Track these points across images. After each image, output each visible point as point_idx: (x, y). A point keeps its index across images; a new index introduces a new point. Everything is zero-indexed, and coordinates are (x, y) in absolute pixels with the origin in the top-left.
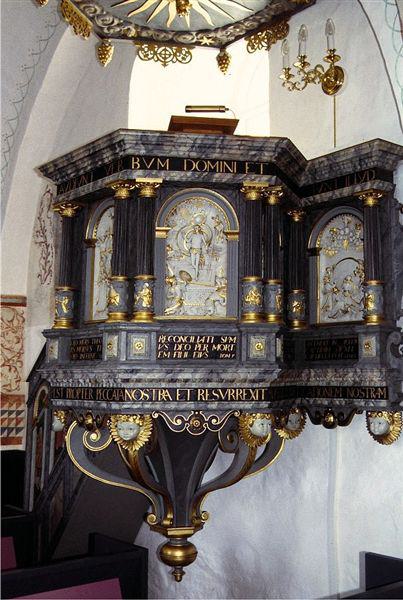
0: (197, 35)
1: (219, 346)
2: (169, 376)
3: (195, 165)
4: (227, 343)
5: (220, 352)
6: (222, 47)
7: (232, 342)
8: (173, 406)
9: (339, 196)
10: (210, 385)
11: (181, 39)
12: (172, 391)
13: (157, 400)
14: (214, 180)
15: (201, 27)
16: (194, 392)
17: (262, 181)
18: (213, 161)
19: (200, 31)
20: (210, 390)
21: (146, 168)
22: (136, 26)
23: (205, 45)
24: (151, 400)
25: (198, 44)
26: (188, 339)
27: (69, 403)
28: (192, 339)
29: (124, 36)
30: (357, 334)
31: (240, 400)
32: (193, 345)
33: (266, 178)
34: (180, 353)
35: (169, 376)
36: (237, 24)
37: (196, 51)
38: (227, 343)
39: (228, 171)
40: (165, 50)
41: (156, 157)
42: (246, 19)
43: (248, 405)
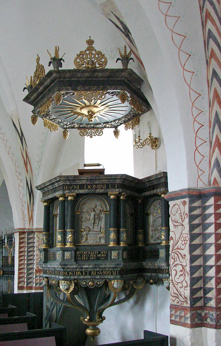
0: (104, 124)
1: (100, 255)
2: (80, 266)
3: (89, 187)
4: (103, 254)
5: (100, 257)
6: (116, 127)
7: (105, 253)
8: (82, 277)
9: (152, 193)
10: (96, 270)
11: (97, 126)
12: (82, 272)
13: (76, 275)
14: (97, 192)
15: (105, 122)
16: (90, 272)
17: (117, 191)
18: (96, 185)
19: (104, 123)
20: (96, 272)
21: (70, 189)
22: (77, 124)
23: (108, 127)
24: (73, 275)
25: (105, 127)
26: (88, 253)
27: (47, 276)
28: (89, 253)
29: (73, 127)
30: (158, 248)
31: (108, 275)
32: (90, 255)
33: (117, 190)
34: (84, 258)
35: (80, 266)
36: (119, 119)
37: (105, 130)
38: (103, 254)
39: (102, 188)
40: (91, 131)
41: (74, 185)
42: (122, 118)
43: (112, 277)
